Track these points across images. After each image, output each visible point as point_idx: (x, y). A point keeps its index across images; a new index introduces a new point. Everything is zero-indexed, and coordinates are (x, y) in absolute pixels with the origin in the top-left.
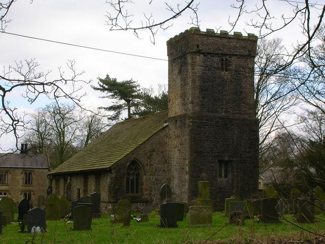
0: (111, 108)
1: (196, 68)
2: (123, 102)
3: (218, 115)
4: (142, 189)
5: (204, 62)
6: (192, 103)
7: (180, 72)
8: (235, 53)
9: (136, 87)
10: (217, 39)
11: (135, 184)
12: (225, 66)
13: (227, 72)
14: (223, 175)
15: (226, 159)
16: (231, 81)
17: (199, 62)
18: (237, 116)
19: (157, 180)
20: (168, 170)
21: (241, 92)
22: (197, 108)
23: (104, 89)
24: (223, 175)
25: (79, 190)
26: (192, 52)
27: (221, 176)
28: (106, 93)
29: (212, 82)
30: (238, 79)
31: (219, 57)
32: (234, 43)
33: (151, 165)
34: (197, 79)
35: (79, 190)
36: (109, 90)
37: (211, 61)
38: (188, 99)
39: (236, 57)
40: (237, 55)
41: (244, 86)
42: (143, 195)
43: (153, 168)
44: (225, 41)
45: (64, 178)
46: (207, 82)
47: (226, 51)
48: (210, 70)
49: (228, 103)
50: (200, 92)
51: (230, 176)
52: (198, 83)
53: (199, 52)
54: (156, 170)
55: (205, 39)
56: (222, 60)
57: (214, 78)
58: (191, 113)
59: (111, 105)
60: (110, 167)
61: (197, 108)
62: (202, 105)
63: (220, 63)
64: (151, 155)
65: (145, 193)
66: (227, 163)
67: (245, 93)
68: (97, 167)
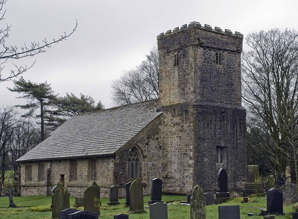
0: (27, 107)
1: (197, 60)
2: (36, 101)
3: (216, 105)
4: (141, 174)
5: (204, 55)
6: (195, 92)
7: (177, 63)
8: (227, 48)
9: (48, 90)
10: (213, 34)
11: (134, 169)
12: (219, 60)
13: (221, 65)
14: (219, 160)
15: (223, 145)
16: (224, 74)
17: (200, 54)
18: (229, 106)
19: (153, 165)
20: (163, 156)
21: (232, 84)
22: (199, 98)
23: (19, 90)
24: (219, 160)
25: (62, 176)
26: (194, 45)
27: (218, 162)
28: (22, 94)
29: (210, 74)
30: (230, 73)
31: (215, 51)
32: (225, 39)
33: (149, 151)
34: (199, 70)
35: (62, 176)
36: (26, 91)
37: (209, 54)
38: (190, 89)
39: (227, 52)
40: (228, 50)
41: (233, 78)
42: (142, 180)
43: (150, 154)
44: (219, 36)
45: (39, 164)
46: (206, 73)
47: (220, 46)
48: (208, 62)
49: (223, 94)
50: (200, 83)
51: (225, 161)
52: (199, 74)
53: (201, 45)
54: (153, 156)
55: (204, 32)
56: (217, 54)
57: (212, 70)
58: (195, 102)
59: (25, 104)
60: (115, 153)
61: (199, 98)
62: (203, 94)
63: (215, 57)
64: (148, 142)
65: (144, 177)
66: (222, 148)
67: (235, 85)
68: (92, 153)
